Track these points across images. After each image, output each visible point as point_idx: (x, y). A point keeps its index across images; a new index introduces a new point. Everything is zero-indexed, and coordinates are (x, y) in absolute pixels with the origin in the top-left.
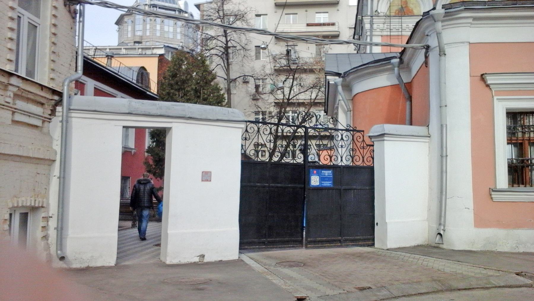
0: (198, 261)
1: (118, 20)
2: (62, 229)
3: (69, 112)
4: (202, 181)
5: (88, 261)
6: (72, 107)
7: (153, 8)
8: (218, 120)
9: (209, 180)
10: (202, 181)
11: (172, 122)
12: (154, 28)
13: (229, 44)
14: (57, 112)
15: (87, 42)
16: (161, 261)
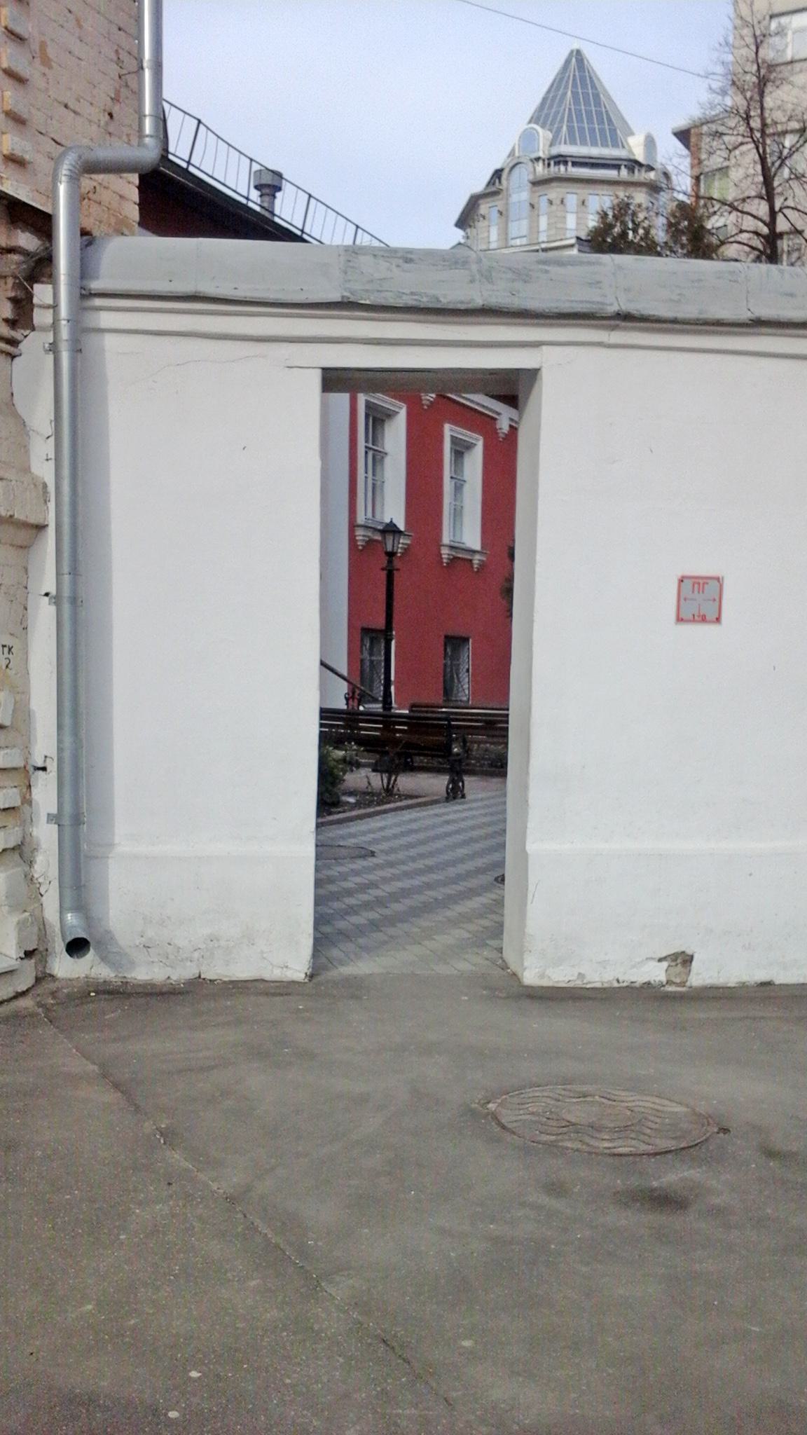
0: (663, 978)
1: (463, 213)
2: (77, 820)
3: (85, 309)
4: (680, 620)
5: (196, 955)
6: (95, 285)
7: (557, 168)
8: (759, 324)
9: (711, 615)
10: (680, 620)
11: (537, 345)
12: (559, 225)
13: (782, 225)
14: (41, 307)
15: (318, 200)
16: (505, 967)
